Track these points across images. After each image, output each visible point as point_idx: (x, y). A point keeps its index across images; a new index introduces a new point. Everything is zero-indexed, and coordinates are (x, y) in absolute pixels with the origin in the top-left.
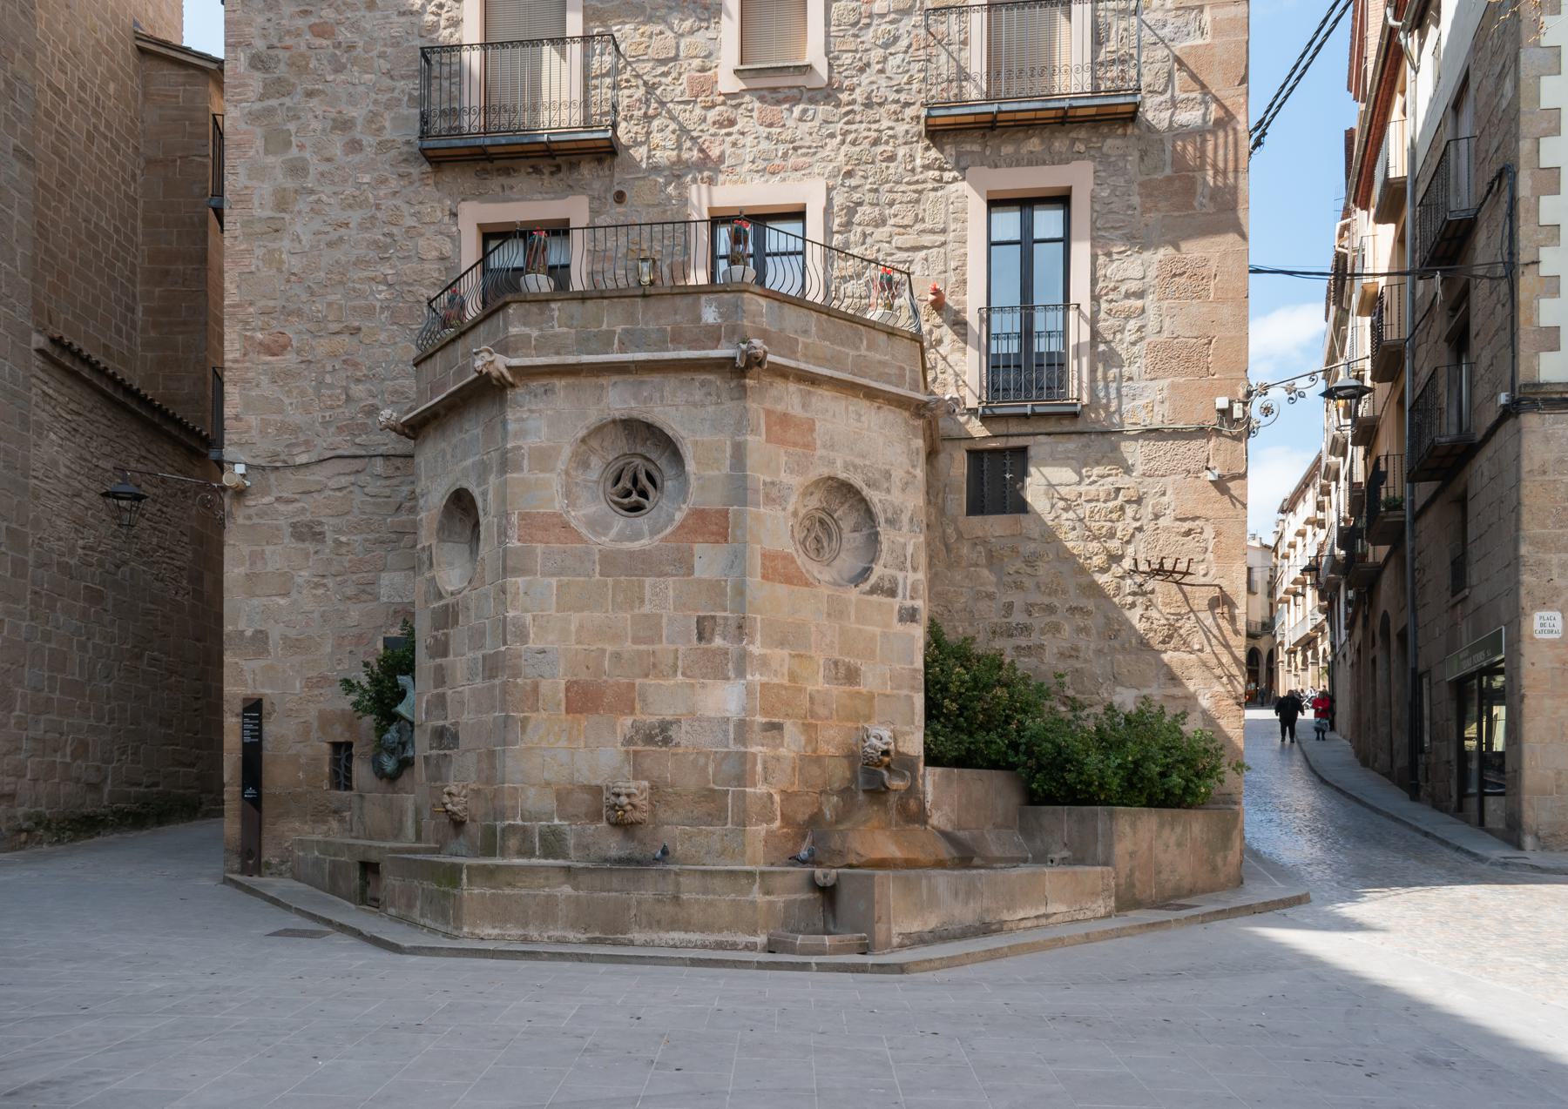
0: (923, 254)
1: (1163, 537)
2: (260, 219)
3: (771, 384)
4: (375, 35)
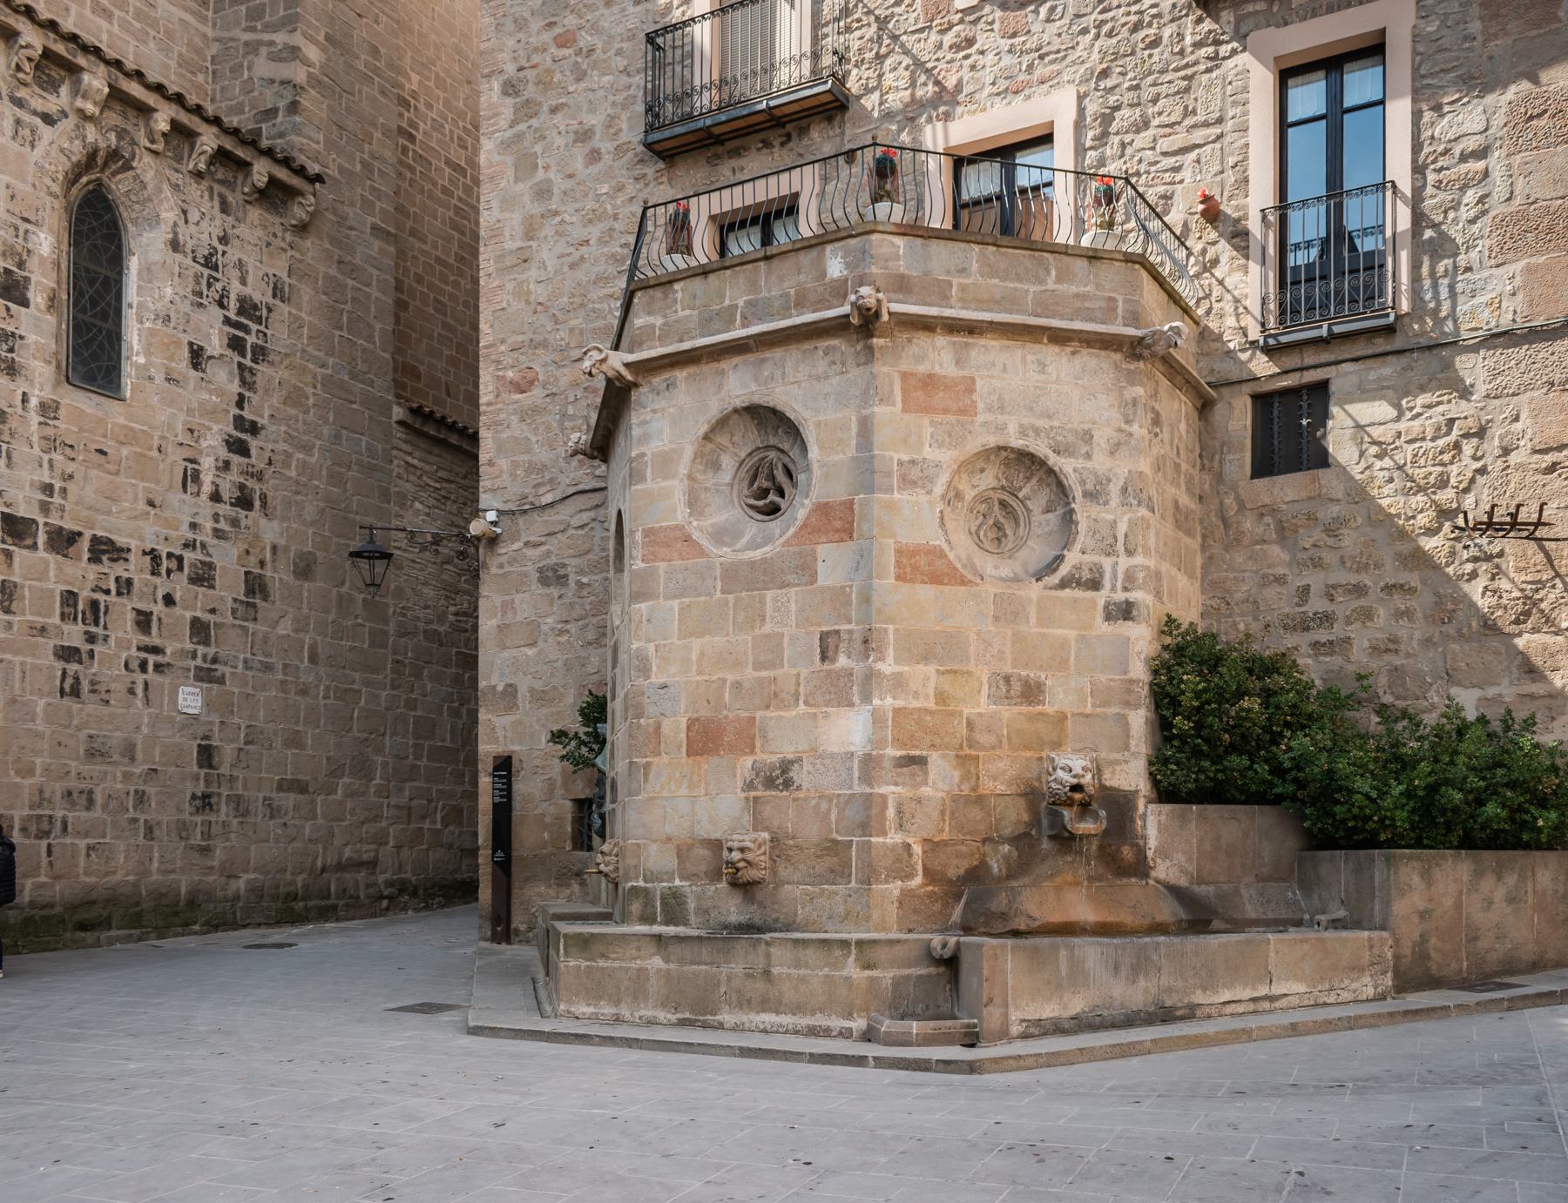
0: (1193, 155)
1: (1515, 478)
2: (511, 252)
3: (909, 340)
4: (613, 32)
